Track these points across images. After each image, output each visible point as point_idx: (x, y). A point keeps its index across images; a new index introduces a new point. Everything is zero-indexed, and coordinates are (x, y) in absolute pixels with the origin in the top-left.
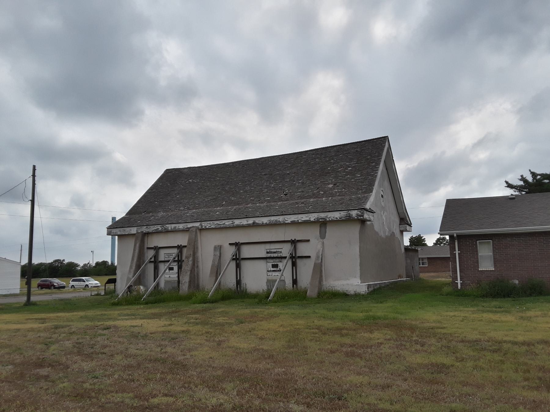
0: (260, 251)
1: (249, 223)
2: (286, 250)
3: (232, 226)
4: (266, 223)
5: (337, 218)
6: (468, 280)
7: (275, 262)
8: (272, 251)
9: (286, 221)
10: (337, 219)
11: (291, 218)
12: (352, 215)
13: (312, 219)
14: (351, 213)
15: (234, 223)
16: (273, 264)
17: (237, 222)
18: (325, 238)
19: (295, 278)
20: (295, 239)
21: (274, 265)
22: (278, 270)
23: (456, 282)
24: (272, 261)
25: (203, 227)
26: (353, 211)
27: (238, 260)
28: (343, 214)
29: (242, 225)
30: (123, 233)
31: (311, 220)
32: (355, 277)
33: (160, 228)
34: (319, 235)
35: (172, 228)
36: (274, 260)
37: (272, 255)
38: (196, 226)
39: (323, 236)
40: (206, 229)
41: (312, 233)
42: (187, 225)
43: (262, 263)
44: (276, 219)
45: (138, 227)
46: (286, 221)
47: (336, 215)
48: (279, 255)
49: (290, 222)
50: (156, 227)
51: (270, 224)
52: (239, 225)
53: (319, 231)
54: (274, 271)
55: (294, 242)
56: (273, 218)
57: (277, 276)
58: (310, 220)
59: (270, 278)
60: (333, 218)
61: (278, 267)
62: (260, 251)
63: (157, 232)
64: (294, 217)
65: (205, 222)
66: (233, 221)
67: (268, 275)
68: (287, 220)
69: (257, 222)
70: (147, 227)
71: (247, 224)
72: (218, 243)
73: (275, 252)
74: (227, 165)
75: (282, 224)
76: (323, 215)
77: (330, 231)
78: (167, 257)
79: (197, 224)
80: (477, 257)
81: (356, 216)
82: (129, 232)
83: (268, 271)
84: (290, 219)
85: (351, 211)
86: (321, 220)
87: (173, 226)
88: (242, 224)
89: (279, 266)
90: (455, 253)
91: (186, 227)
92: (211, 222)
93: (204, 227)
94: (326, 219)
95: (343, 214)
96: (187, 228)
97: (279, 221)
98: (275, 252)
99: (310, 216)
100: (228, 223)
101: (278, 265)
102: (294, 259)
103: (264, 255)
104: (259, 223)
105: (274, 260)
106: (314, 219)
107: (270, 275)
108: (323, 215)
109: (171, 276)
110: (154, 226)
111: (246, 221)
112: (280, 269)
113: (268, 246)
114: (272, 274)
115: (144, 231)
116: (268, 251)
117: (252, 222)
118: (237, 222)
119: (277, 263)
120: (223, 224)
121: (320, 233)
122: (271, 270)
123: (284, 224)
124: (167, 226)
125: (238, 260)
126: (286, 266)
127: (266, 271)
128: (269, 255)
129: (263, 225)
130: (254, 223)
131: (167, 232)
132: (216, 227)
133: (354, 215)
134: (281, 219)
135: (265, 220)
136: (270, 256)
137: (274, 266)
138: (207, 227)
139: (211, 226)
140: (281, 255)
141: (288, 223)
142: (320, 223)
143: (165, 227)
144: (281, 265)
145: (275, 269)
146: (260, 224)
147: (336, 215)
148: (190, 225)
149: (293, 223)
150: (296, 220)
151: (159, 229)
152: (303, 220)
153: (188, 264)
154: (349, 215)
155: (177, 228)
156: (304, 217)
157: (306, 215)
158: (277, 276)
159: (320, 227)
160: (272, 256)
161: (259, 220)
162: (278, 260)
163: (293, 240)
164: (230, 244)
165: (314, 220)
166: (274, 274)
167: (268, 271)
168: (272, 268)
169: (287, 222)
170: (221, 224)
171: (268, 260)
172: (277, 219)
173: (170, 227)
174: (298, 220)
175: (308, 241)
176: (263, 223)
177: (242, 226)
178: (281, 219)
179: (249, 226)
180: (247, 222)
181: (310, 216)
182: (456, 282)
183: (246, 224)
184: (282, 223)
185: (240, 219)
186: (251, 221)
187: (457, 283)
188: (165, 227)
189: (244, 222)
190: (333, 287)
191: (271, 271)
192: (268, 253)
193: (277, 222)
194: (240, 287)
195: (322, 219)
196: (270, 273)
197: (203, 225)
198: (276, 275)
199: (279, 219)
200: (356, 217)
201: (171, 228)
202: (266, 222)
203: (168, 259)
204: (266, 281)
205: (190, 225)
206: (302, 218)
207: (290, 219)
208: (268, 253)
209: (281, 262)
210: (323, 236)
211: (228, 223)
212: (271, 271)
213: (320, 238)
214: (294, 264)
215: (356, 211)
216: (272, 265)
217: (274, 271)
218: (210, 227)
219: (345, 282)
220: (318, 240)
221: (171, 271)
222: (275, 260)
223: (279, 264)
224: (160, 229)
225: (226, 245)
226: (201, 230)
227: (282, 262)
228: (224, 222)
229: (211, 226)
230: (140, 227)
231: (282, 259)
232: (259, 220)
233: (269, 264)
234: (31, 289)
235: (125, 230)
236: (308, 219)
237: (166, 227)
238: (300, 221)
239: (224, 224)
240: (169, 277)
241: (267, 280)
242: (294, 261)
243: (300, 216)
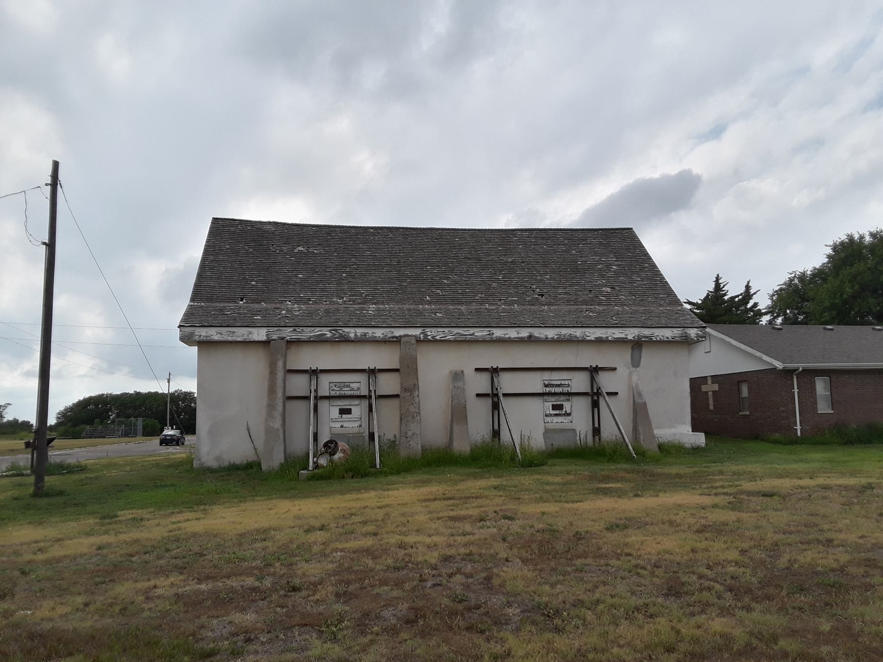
0: (534, 383)
1: (520, 336)
2: (580, 382)
3: (488, 338)
4: (552, 338)
5: (668, 338)
6: (807, 425)
7: (558, 401)
8: (554, 382)
9: (587, 336)
10: (668, 339)
11: (595, 333)
12: (690, 335)
13: (630, 337)
14: (688, 332)
15: (493, 334)
16: (555, 403)
17: (498, 333)
18: (639, 366)
19: (597, 425)
20: (597, 366)
21: (557, 405)
22: (563, 413)
23: (795, 427)
24: (554, 400)
25: (429, 337)
26: (691, 329)
27: (494, 399)
28: (677, 332)
29: (509, 338)
30: (230, 339)
31: (629, 338)
32: (684, 423)
33: (328, 333)
34: (630, 361)
35: (358, 334)
36: (557, 398)
37: (553, 390)
38: (414, 334)
39: (636, 363)
40: (434, 341)
41: (620, 359)
42: (393, 332)
43: (537, 402)
44: (570, 332)
45: (271, 329)
46: (587, 336)
47: (667, 334)
48: (565, 390)
49: (593, 339)
50: (317, 331)
51: (561, 339)
52: (503, 338)
53: (630, 355)
54: (556, 415)
55: (594, 371)
56: (565, 331)
57: (561, 422)
58: (627, 338)
59: (550, 426)
60: (662, 338)
61: (563, 409)
62: (534, 383)
63: (321, 341)
64: (601, 332)
65: (433, 330)
66: (490, 331)
67: (546, 421)
68: (588, 335)
69: (536, 335)
70: (295, 330)
71: (518, 338)
72: (456, 366)
73: (559, 386)
74: (345, 232)
75: (581, 341)
76: (647, 332)
77: (648, 356)
78: (338, 389)
79: (417, 332)
80: (816, 397)
81: (696, 337)
82: (245, 337)
83: (547, 415)
84: (594, 334)
85: (689, 329)
86: (643, 339)
87: (360, 331)
88: (507, 336)
89: (564, 407)
90: (794, 392)
91: (390, 335)
92: (446, 330)
93: (432, 337)
94: (652, 339)
95: (677, 332)
96: (393, 337)
97: (576, 337)
98: (559, 386)
99: (627, 332)
100: (480, 333)
101: (351, 409)
102: (595, 397)
103: (540, 389)
104: (539, 338)
105: (556, 398)
106: (633, 337)
107: (549, 421)
108: (647, 332)
109: (345, 425)
110: (313, 329)
111: (516, 333)
112: (566, 411)
113: (547, 376)
114: (552, 420)
115: (289, 338)
116: (546, 382)
117: (528, 334)
118: (498, 333)
119: (561, 403)
120: (470, 335)
121: (631, 359)
122: (551, 413)
123: (583, 342)
124: (346, 330)
125: (494, 399)
126: (579, 409)
127: (542, 416)
128: (548, 390)
129: (546, 341)
130: (530, 336)
131: (345, 340)
132: (457, 339)
133: (692, 335)
134: (578, 333)
135: (551, 333)
136: (549, 391)
137: (555, 407)
138: (438, 338)
139: (445, 337)
140: (568, 391)
141: (591, 341)
142: (632, 344)
143: (340, 331)
144: (567, 406)
145: (558, 413)
146: (542, 339)
147: (667, 334)
148: (399, 332)
149: (599, 341)
150: (604, 336)
151: (326, 334)
152: (615, 337)
153: (413, 402)
154: (685, 335)
155: (370, 335)
156: (617, 333)
157: (620, 330)
158: (561, 422)
159: (633, 349)
160: (553, 392)
161: (538, 333)
162: (562, 398)
163: (493, 367)
164: (477, 370)
165: (632, 339)
166: (556, 419)
167: (547, 415)
168: (552, 410)
169: (588, 338)
170: (465, 335)
171: (546, 398)
172: (572, 333)
173: (352, 333)
174: (607, 337)
175: (615, 369)
176: (547, 338)
177: (507, 339)
178: (578, 333)
179: (520, 341)
180: (518, 333)
181: (627, 332)
182: (795, 427)
183: (515, 338)
184: (581, 339)
185: (650, 328)
186: (524, 333)
187: (797, 429)
188: (340, 331)
189: (512, 333)
190: (659, 437)
191: (551, 415)
192: (546, 386)
193: (571, 337)
194: (600, 439)
195: (645, 337)
196: (549, 419)
197: (429, 333)
198: (558, 422)
199: (575, 334)
200: (695, 339)
201: (356, 335)
202: (552, 336)
203: (338, 393)
204: (542, 430)
205: (399, 332)
206: (614, 334)
207: (594, 334)
208: (546, 386)
209: (568, 400)
210: (636, 363)
211: (480, 333)
212: (551, 415)
213: (631, 366)
214: (595, 405)
215: (696, 330)
216: (552, 405)
217: (556, 415)
218: (444, 338)
219: (673, 431)
220: (628, 368)
221: (344, 416)
222: (558, 398)
223: (353, 409)
224: (329, 335)
225: (469, 372)
226: (298, 342)
227: (569, 401)
228: (471, 331)
229: (445, 337)
230: (276, 329)
231: (569, 396)
232: (538, 333)
233: (547, 404)
234: (50, 453)
235: (234, 333)
236: (623, 336)
237: (344, 332)
238: (610, 338)
239: (473, 334)
240: (342, 426)
241: (546, 429)
242: (595, 400)
243: (610, 331)
